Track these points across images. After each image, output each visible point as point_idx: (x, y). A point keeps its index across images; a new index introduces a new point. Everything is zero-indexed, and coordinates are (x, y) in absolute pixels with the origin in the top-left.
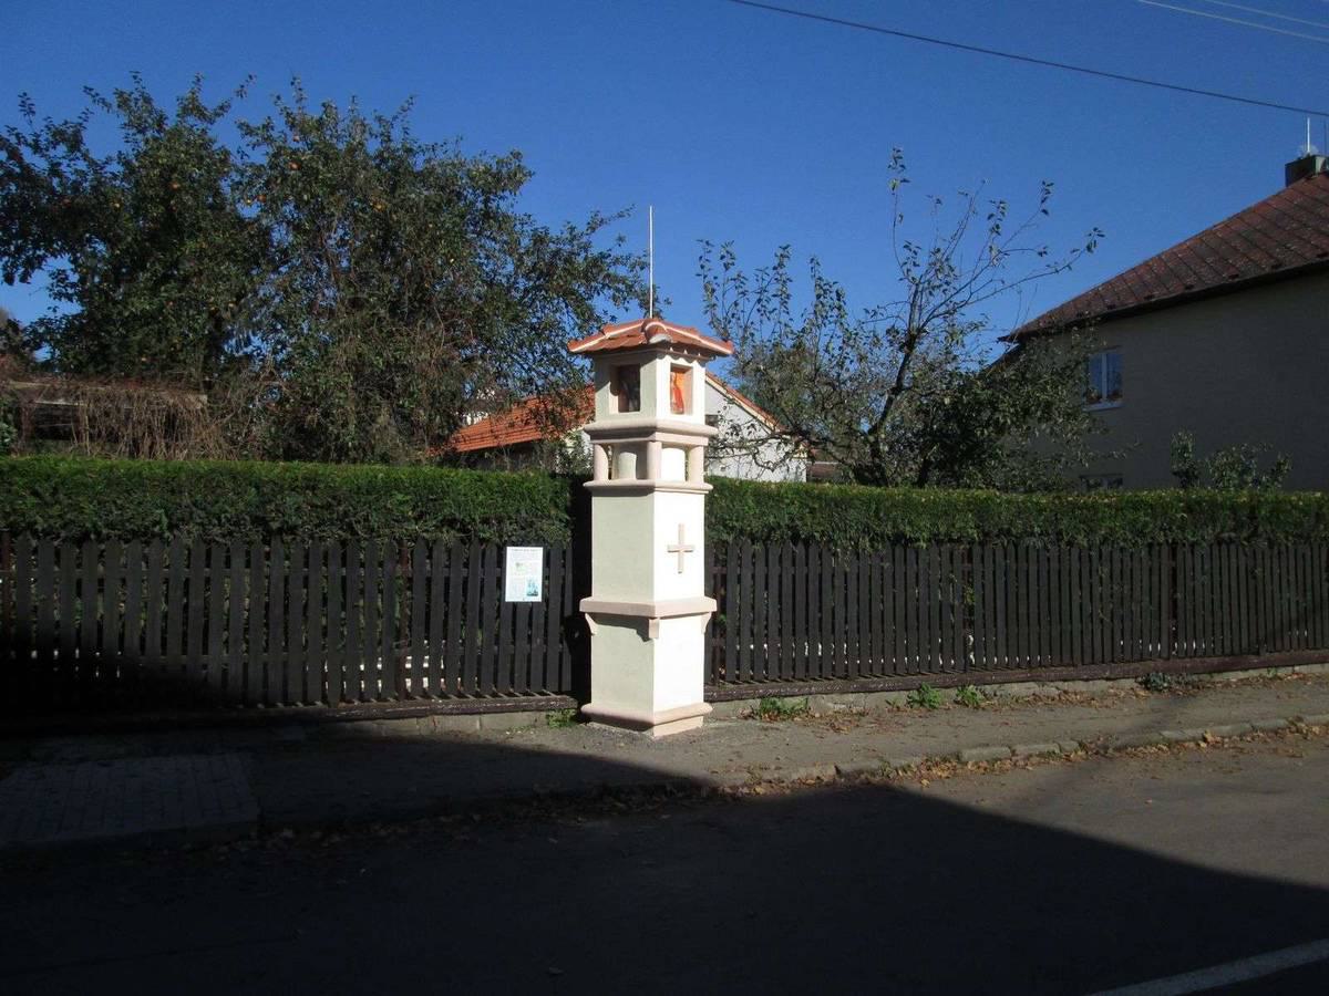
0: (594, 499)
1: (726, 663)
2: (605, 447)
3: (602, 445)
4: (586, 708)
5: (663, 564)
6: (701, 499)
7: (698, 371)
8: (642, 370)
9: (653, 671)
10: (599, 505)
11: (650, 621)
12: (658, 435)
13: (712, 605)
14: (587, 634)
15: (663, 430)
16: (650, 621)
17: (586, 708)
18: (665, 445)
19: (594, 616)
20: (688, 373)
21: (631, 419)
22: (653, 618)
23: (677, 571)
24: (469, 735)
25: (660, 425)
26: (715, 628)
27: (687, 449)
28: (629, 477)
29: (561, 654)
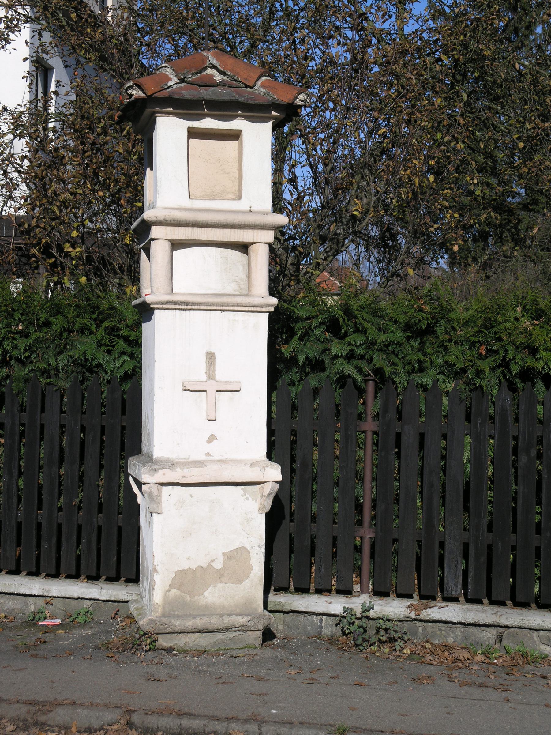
13: (274, 473)
15: (172, 465)
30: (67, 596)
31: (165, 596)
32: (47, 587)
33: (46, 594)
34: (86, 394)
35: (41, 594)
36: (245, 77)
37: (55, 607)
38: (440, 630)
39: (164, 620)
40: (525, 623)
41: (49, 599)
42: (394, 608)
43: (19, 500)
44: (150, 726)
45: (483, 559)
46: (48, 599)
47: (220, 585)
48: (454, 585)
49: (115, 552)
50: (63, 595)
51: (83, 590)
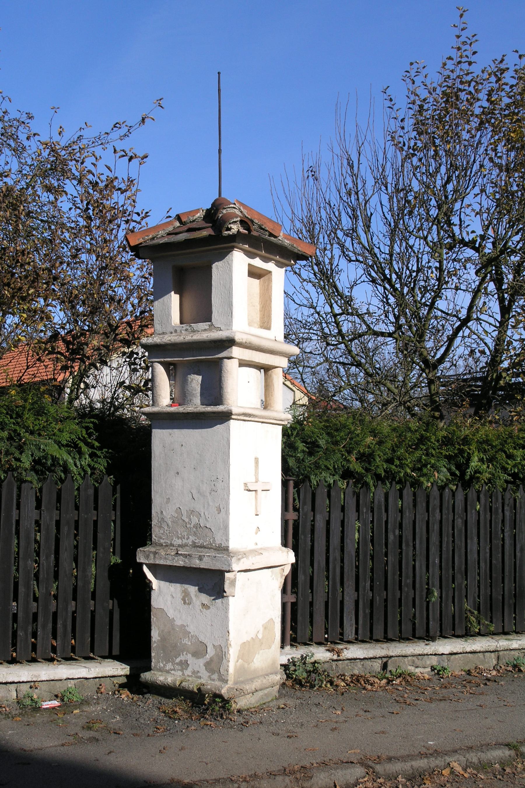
0: (153, 430)
1: (296, 625)
2: (166, 366)
3: (161, 363)
4: (146, 676)
5: (239, 504)
6: (279, 430)
7: (278, 275)
8: (214, 266)
9: (193, 429)
10: (161, 439)
11: (227, 575)
12: (236, 351)
13: (289, 557)
14: (147, 587)
15: (245, 554)
16: (227, 575)
17: (146, 676)
18: (243, 364)
19: (153, 568)
20: (266, 277)
21: (202, 333)
22: (229, 571)
23: (254, 513)
24: (31, 751)
25: (238, 338)
26: (293, 583)
27: (266, 369)
28: (196, 405)
29: (111, 613)
30: (56, 678)
31: (236, 665)
32: (36, 673)
33: (35, 679)
34: (76, 493)
35: (30, 680)
36: (272, 227)
37: (40, 690)
38: (347, 666)
39: (239, 686)
40: (404, 653)
41: (32, 684)
42: (320, 654)
43: (94, 594)
44: (390, 772)
45: (368, 611)
46: (33, 684)
47: (261, 652)
48: (319, 633)
49: (89, 634)
50: (52, 678)
51: (74, 671)
